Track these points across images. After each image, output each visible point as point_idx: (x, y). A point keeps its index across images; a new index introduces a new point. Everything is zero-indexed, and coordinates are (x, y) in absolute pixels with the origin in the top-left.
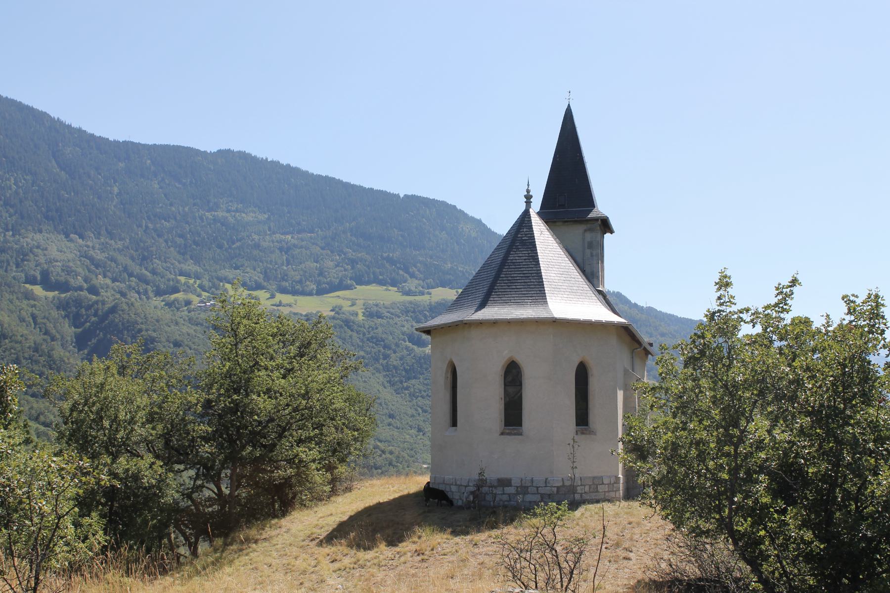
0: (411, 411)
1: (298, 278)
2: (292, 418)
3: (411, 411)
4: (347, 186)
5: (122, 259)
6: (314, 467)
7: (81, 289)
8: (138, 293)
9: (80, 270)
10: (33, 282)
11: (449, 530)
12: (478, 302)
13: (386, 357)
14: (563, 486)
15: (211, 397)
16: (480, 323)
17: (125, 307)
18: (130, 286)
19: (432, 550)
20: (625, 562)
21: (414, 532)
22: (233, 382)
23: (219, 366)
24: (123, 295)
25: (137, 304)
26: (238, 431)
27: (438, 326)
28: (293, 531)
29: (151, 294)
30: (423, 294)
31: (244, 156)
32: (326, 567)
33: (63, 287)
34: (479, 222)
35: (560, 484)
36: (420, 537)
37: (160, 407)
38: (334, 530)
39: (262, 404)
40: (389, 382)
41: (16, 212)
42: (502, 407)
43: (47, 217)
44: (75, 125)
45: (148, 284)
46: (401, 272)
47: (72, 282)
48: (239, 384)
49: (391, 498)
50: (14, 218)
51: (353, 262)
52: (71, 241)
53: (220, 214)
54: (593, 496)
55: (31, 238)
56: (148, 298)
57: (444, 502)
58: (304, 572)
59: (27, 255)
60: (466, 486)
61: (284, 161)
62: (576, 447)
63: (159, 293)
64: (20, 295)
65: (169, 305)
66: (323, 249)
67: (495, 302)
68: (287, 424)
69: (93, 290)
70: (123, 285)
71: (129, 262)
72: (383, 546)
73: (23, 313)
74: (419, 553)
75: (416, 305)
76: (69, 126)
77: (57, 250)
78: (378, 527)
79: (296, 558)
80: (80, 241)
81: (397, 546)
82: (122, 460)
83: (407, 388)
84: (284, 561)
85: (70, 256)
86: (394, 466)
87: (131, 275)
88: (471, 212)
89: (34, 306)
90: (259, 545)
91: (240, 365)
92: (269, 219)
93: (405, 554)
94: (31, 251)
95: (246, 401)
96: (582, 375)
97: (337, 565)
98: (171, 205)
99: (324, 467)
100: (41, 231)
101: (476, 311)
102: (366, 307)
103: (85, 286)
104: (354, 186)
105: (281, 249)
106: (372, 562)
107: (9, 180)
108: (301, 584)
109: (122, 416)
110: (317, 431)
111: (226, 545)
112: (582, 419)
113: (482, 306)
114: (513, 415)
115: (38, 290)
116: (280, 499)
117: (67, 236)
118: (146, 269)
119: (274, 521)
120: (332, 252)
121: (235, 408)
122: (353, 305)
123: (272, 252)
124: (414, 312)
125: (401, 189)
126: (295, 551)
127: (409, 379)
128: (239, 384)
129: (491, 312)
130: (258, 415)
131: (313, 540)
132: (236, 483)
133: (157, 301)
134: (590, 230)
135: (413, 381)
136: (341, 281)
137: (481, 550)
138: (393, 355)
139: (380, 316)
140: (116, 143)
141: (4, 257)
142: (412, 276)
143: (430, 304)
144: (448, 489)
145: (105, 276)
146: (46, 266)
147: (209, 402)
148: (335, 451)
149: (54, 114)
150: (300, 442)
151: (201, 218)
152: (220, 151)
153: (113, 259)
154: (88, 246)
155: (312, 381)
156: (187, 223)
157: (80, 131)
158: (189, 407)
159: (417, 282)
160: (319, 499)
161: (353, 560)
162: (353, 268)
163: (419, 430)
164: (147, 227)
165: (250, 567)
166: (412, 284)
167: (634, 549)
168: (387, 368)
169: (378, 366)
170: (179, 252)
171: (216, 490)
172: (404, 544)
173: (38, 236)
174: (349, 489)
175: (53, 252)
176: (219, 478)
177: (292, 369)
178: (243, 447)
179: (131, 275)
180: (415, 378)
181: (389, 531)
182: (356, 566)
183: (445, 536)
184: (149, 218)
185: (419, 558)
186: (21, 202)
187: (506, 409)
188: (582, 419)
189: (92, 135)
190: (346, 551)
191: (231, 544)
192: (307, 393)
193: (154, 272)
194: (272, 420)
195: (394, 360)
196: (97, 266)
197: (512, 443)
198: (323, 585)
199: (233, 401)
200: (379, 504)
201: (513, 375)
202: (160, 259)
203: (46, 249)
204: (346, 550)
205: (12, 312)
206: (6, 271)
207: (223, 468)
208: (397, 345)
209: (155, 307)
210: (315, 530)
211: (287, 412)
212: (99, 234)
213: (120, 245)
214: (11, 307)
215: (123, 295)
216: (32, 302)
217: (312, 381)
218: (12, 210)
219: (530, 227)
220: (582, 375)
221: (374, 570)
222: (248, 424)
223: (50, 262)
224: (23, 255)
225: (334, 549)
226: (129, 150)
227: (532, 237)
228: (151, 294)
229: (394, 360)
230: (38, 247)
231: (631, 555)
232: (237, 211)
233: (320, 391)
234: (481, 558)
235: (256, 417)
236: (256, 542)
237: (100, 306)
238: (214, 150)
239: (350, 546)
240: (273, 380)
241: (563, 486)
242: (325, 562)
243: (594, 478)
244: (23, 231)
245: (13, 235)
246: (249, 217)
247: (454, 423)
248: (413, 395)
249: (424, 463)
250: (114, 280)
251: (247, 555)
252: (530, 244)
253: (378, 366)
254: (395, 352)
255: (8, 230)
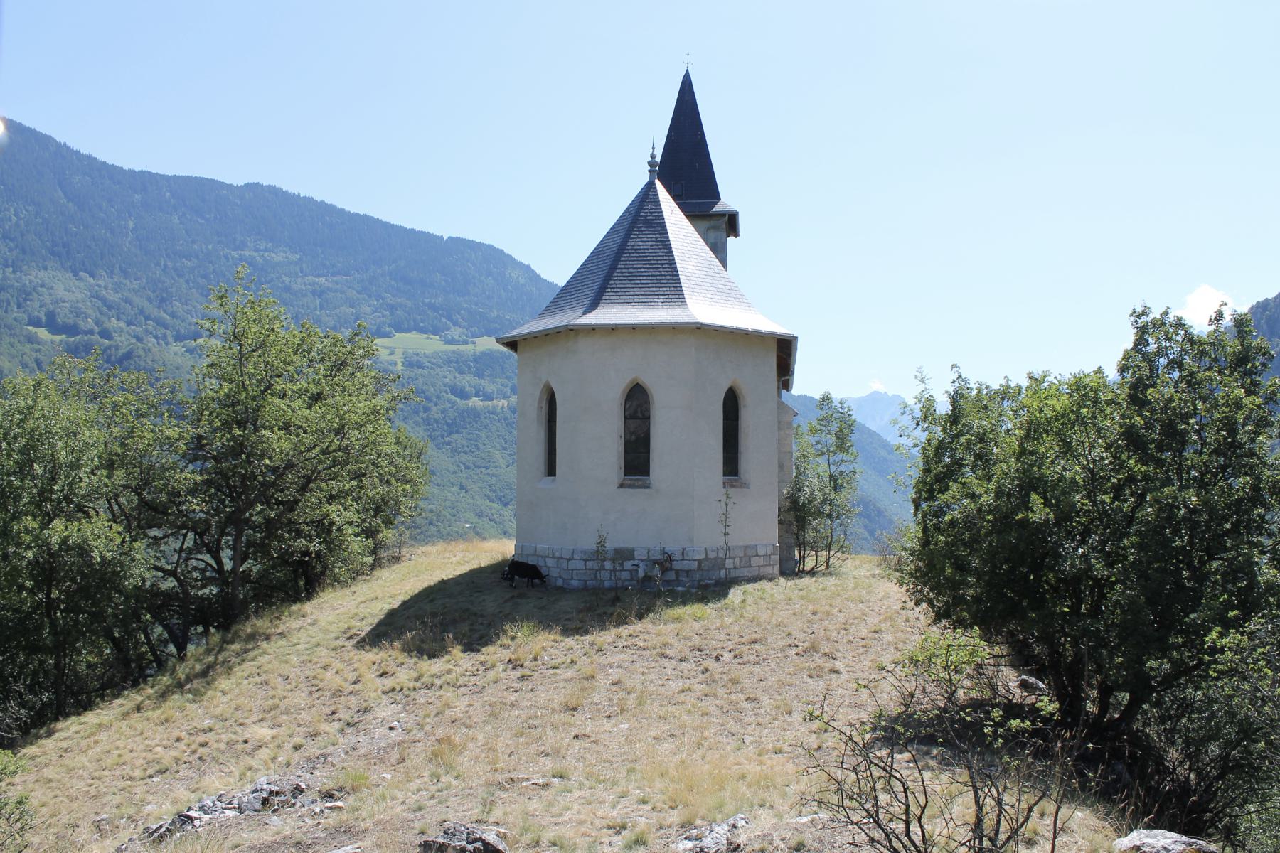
0: (452, 468)
1: (332, 324)
2: (320, 462)
3: (452, 468)
4: (387, 225)
5: (140, 301)
6: (350, 531)
7: (91, 332)
8: (156, 337)
9: (90, 312)
10: (38, 324)
11: (559, 628)
12: (587, 301)
13: (427, 410)
14: (707, 558)
15: (200, 431)
16: (593, 329)
17: (141, 353)
18: (147, 331)
19: (536, 659)
20: (834, 676)
21: (505, 632)
22: (234, 412)
23: (214, 387)
24: (139, 339)
25: (155, 350)
26: (243, 482)
27: (530, 334)
28: (323, 623)
29: (170, 340)
30: (467, 343)
31: (274, 191)
32: (373, 685)
33: (71, 330)
34: (528, 267)
35: (703, 556)
36: (513, 638)
37: (123, 445)
38: (381, 623)
39: (278, 444)
40: (430, 436)
41: (17, 246)
42: (622, 448)
43: (53, 253)
44: (84, 151)
45: (166, 328)
46: (444, 320)
47: (82, 325)
48: (242, 414)
49: (458, 573)
50: (14, 253)
51: (392, 308)
52: (81, 279)
53: (247, 253)
54: (745, 572)
55: (33, 276)
56: (167, 344)
57: (537, 581)
58: (338, 693)
59: (30, 294)
60: (568, 560)
61: (318, 198)
62: (731, 504)
63: (179, 338)
64: (22, 338)
65: (190, 351)
66: (359, 293)
67: (612, 301)
68: (313, 472)
69: (105, 334)
70: (138, 329)
71: (146, 304)
72: (457, 651)
73: (26, 358)
74: (514, 664)
75: (460, 354)
76: (78, 153)
77: (65, 290)
78: (444, 620)
79: (325, 668)
80: (91, 280)
81: (478, 651)
82: (58, 524)
83: (449, 443)
84: (308, 673)
85: (79, 296)
86: (435, 526)
87: (147, 318)
88: (520, 257)
89: (38, 351)
90: (273, 644)
91: (246, 389)
92: (300, 259)
93: (493, 666)
94: (35, 290)
95: (253, 438)
96: (732, 403)
97: (389, 682)
98: (193, 242)
99: (363, 531)
100: (46, 269)
101: (585, 313)
102: (406, 356)
103: (97, 329)
104: (393, 226)
105: (314, 293)
106: (443, 679)
107: (8, 210)
108: (334, 713)
109: (62, 456)
110: (354, 483)
111: (225, 641)
112: (731, 465)
113: (593, 305)
114: (637, 460)
115: (43, 333)
116: (302, 579)
117: (76, 274)
118: (165, 312)
119: (294, 608)
120: (370, 296)
121: (238, 449)
122: (391, 354)
123: (304, 296)
124: (457, 362)
125: (445, 230)
126: (323, 655)
127: (451, 433)
128: (242, 414)
129: (606, 315)
130: (270, 458)
131: (351, 637)
132: (240, 558)
133: (177, 347)
134: (715, 228)
135: (456, 436)
136: (379, 329)
137: (611, 659)
138: (434, 408)
139: (420, 366)
140: (131, 172)
141: (4, 296)
142: (455, 324)
143: (474, 354)
144: (541, 563)
145: (118, 319)
146: (51, 307)
147: (199, 438)
148: (378, 510)
149: (61, 138)
150: (331, 498)
151: (226, 257)
152: (247, 185)
153: (127, 301)
154: (99, 286)
155: (349, 411)
156: (211, 262)
157: (90, 158)
158: (168, 444)
159: (461, 330)
160: (357, 574)
161: (415, 675)
162: (392, 314)
163: (462, 488)
164: (166, 266)
165: (258, 679)
166: (455, 332)
167: (838, 655)
168: (427, 422)
169: (417, 419)
170: (202, 294)
171: (214, 565)
172: (490, 649)
173: (42, 274)
174: (396, 559)
175: (60, 291)
176: (219, 548)
177: (319, 394)
178: (251, 505)
179: (147, 318)
180: (457, 432)
181: (465, 628)
182: (418, 685)
183: (552, 637)
184: (168, 255)
185: (518, 673)
186: (22, 235)
187: (626, 452)
188: (731, 465)
189: (104, 163)
190: (400, 660)
191: (232, 642)
192: (342, 427)
193: (173, 315)
194: (290, 466)
195: (435, 413)
196: (110, 308)
197: (635, 499)
198: (369, 717)
199: (233, 438)
200: (443, 582)
201: (637, 404)
202: (180, 301)
203: (52, 288)
204: (402, 657)
205: (13, 356)
206: (6, 311)
207: (222, 533)
208: (438, 397)
209: (175, 354)
210: (353, 623)
211: (313, 454)
212: (112, 272)
213: (135, 285)
214: (12, 351)
215: (139, 339)
216: (36, 346)
217: (349, 411)
218: (11, 244)
219: (658, 204)
220: (732, 403)
221: (448, 694)
222: (257, 471)
223: (57, 302)
224: (25, 295)
225: (382, 654)
226: (145, 180)
227: (661, 217)
228: (170, 340)
229: (435, 413)
230: (42, 286)
231: (838, 665)
232: (266, 250)
233: (359, 426)
234: (615, 674)
235: (267, 461)
236: (267, 638)
237: (113, 351)
238: (241, 183)
239: (407, 649)
240: (293, 411)
241: (707, 558)
242: (370, 675)
243: (747, 547)
244: (25, 268)
245: (14, 272)
246: (279, 257)
247: (551, 470)
248: (454, 451)
249: (467, 522)
250: (129, 323)
251: (252, 660)
252: (659, 226)
253: (417, 419)
254: (436, 405)
255: (7, 266)
